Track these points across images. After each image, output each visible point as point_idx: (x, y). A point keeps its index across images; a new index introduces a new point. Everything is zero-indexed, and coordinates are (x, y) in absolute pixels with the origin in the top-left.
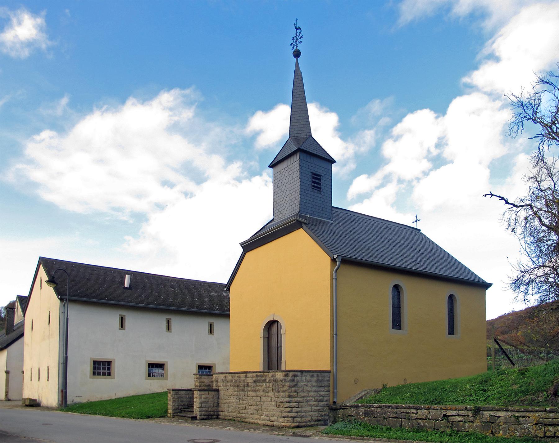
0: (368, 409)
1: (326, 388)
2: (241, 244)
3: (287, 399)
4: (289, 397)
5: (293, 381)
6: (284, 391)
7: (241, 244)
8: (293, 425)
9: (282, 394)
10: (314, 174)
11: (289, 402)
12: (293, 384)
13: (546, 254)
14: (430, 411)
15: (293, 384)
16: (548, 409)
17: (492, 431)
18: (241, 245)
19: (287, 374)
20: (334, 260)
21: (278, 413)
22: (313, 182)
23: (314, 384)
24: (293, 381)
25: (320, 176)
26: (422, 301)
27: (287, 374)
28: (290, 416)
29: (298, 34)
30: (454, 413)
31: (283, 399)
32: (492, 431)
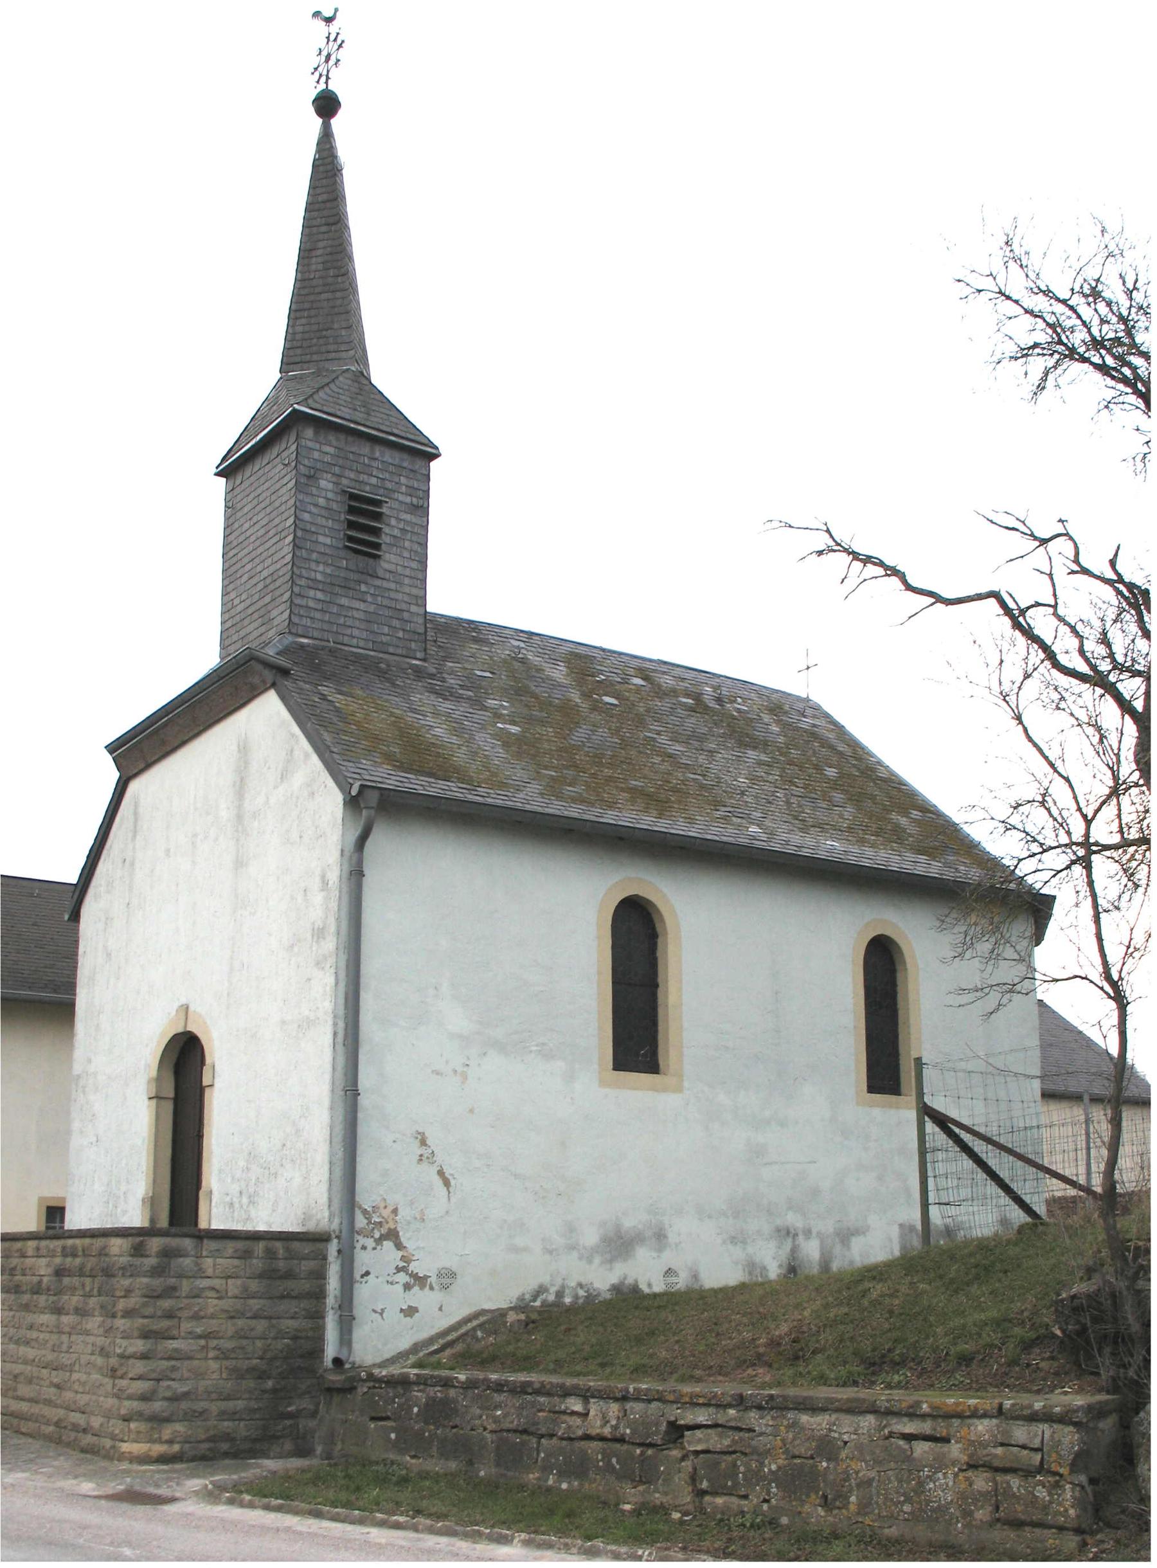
0: (437, 1392)
1: (304, 1304)
2: (112, 748)
3: (139, 1346)
4: (146, 1335)
5: (157, 1271)
6: (128, 1314)
7: (112, 748)
8: (158, 1449)
9: (120, 1323)
10: (353, 497)
11: (144, 1357)
12: (157, 1283)
13: (663, 761)
14: (628, 1405)
15: (157, 1283)
16: (1007, 1404)
17: (825, 1497)
18: (111, 753)
19: (141, 1244)
20: (353, 803)
21: (111, 1402)
22: (351, 525)
23: (254, 1286)
24: (157, 1271)
25: (378, 503)
26: (760, 966)
27: (141, 1244)
28: (147, 1412)
29: (332, 38)
30: (702, 1417)
31: (125, 1343)
32: (825, 1497)
